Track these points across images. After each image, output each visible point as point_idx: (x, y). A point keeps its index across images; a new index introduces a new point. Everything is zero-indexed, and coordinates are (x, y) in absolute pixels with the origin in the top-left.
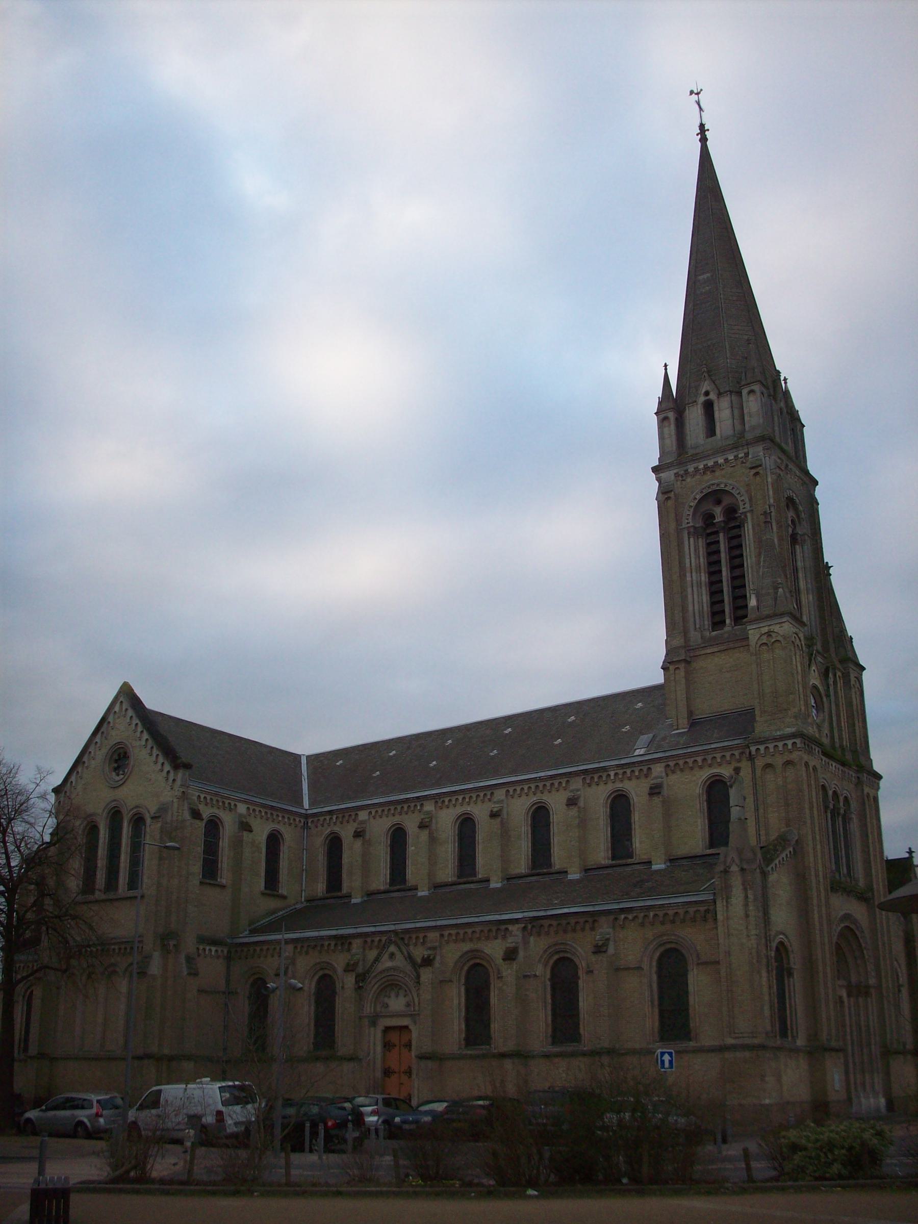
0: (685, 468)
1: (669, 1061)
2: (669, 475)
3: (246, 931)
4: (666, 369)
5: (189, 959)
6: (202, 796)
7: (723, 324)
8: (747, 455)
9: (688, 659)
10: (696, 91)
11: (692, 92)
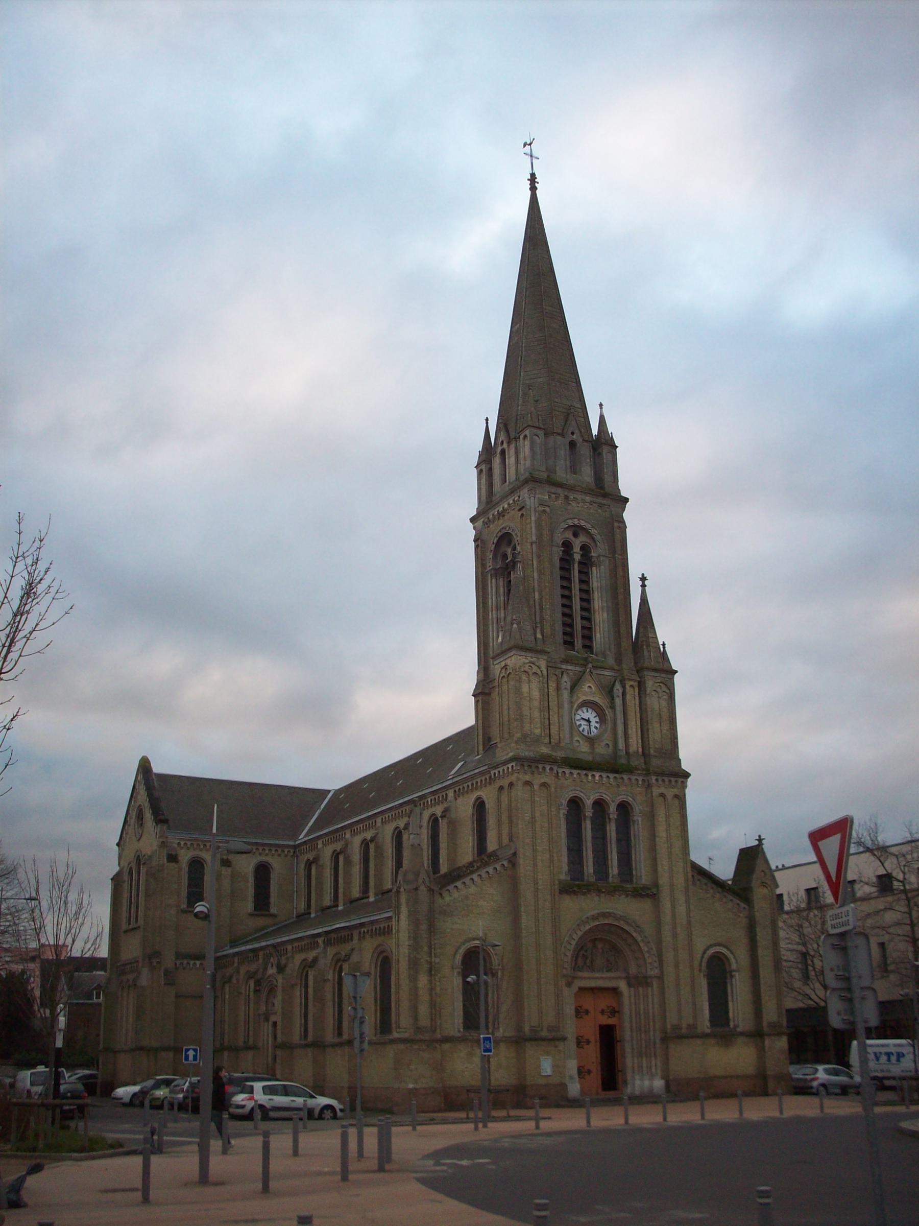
0: (487, 516)
1: (194, 1056)
2: (479, 523)
3: (227, 946)
4: (487, 423)
5: (167, 973)
6: (182, 843)
7: (520, 372)
9: (487, 691)
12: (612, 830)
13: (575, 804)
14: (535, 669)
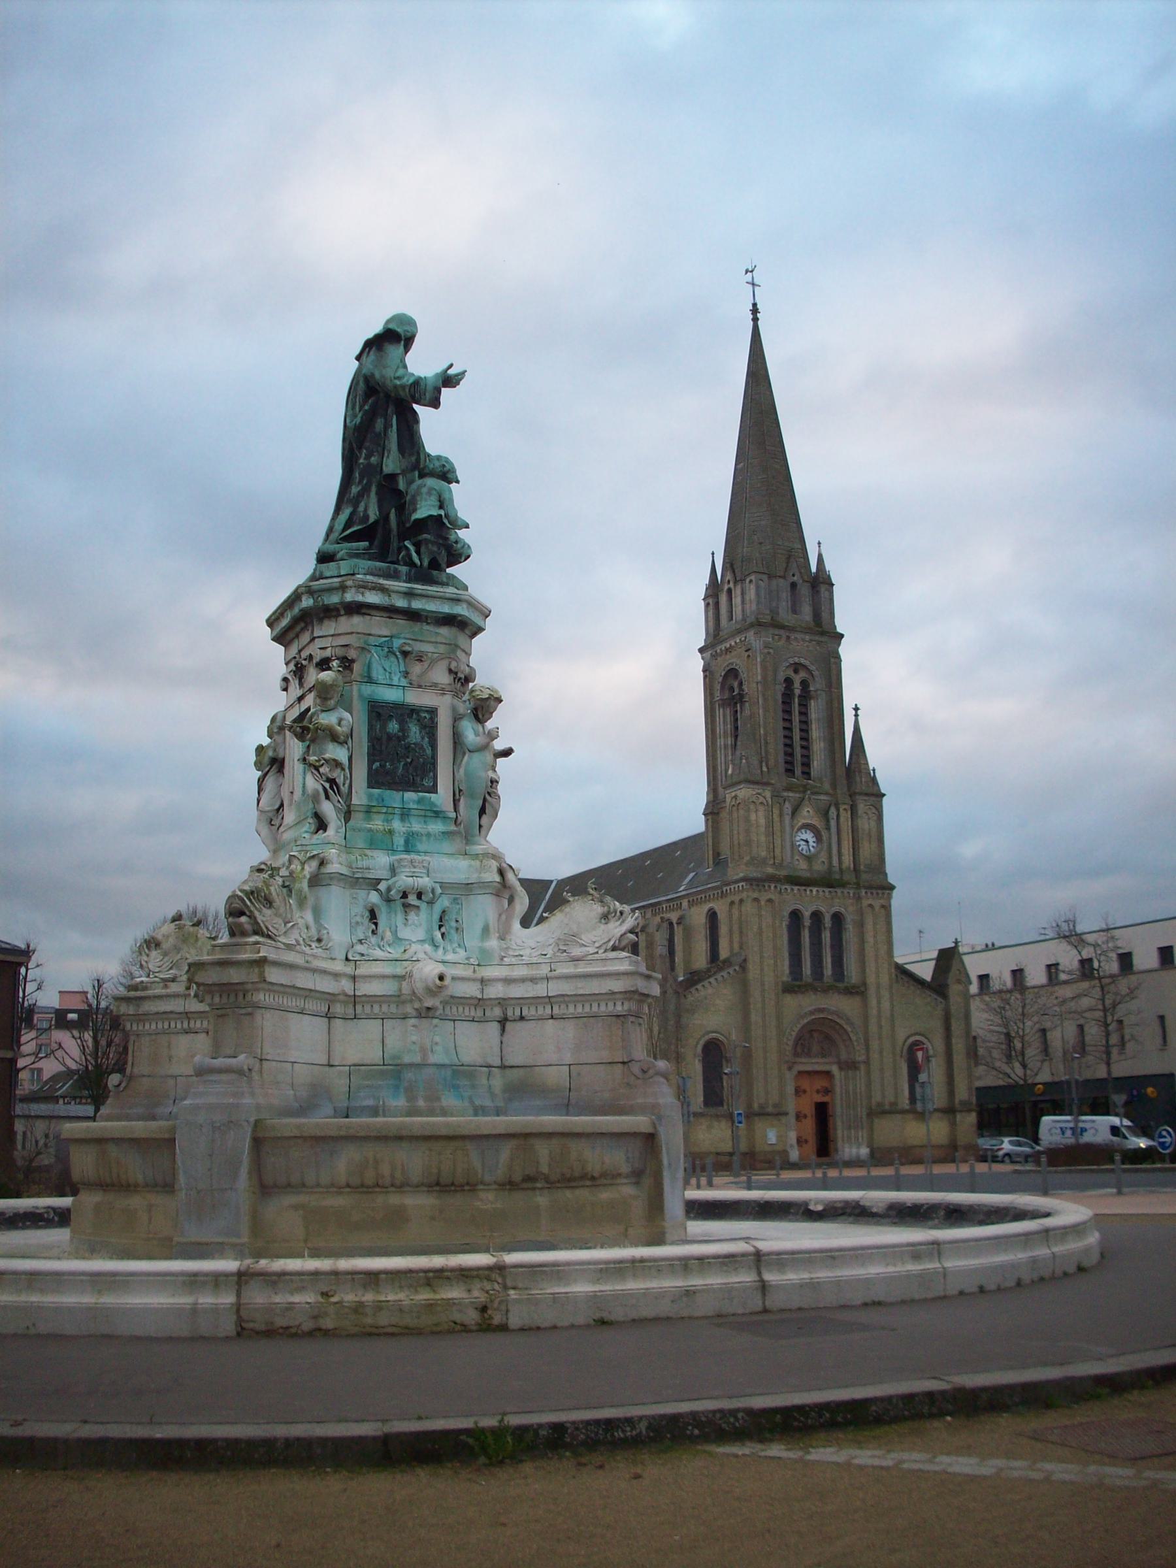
2: (708, 655)
8: (746, 637)
10: (750, 269)
11: (747, 271)
12: (826, 936)
13: (795, 916)
14: (761, 799)
